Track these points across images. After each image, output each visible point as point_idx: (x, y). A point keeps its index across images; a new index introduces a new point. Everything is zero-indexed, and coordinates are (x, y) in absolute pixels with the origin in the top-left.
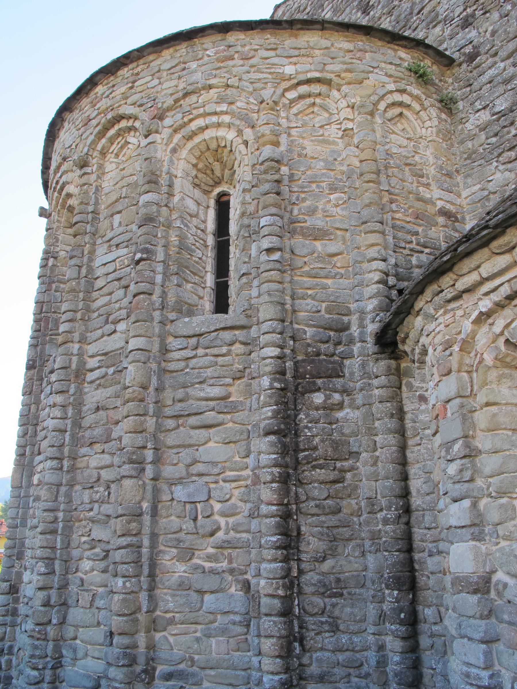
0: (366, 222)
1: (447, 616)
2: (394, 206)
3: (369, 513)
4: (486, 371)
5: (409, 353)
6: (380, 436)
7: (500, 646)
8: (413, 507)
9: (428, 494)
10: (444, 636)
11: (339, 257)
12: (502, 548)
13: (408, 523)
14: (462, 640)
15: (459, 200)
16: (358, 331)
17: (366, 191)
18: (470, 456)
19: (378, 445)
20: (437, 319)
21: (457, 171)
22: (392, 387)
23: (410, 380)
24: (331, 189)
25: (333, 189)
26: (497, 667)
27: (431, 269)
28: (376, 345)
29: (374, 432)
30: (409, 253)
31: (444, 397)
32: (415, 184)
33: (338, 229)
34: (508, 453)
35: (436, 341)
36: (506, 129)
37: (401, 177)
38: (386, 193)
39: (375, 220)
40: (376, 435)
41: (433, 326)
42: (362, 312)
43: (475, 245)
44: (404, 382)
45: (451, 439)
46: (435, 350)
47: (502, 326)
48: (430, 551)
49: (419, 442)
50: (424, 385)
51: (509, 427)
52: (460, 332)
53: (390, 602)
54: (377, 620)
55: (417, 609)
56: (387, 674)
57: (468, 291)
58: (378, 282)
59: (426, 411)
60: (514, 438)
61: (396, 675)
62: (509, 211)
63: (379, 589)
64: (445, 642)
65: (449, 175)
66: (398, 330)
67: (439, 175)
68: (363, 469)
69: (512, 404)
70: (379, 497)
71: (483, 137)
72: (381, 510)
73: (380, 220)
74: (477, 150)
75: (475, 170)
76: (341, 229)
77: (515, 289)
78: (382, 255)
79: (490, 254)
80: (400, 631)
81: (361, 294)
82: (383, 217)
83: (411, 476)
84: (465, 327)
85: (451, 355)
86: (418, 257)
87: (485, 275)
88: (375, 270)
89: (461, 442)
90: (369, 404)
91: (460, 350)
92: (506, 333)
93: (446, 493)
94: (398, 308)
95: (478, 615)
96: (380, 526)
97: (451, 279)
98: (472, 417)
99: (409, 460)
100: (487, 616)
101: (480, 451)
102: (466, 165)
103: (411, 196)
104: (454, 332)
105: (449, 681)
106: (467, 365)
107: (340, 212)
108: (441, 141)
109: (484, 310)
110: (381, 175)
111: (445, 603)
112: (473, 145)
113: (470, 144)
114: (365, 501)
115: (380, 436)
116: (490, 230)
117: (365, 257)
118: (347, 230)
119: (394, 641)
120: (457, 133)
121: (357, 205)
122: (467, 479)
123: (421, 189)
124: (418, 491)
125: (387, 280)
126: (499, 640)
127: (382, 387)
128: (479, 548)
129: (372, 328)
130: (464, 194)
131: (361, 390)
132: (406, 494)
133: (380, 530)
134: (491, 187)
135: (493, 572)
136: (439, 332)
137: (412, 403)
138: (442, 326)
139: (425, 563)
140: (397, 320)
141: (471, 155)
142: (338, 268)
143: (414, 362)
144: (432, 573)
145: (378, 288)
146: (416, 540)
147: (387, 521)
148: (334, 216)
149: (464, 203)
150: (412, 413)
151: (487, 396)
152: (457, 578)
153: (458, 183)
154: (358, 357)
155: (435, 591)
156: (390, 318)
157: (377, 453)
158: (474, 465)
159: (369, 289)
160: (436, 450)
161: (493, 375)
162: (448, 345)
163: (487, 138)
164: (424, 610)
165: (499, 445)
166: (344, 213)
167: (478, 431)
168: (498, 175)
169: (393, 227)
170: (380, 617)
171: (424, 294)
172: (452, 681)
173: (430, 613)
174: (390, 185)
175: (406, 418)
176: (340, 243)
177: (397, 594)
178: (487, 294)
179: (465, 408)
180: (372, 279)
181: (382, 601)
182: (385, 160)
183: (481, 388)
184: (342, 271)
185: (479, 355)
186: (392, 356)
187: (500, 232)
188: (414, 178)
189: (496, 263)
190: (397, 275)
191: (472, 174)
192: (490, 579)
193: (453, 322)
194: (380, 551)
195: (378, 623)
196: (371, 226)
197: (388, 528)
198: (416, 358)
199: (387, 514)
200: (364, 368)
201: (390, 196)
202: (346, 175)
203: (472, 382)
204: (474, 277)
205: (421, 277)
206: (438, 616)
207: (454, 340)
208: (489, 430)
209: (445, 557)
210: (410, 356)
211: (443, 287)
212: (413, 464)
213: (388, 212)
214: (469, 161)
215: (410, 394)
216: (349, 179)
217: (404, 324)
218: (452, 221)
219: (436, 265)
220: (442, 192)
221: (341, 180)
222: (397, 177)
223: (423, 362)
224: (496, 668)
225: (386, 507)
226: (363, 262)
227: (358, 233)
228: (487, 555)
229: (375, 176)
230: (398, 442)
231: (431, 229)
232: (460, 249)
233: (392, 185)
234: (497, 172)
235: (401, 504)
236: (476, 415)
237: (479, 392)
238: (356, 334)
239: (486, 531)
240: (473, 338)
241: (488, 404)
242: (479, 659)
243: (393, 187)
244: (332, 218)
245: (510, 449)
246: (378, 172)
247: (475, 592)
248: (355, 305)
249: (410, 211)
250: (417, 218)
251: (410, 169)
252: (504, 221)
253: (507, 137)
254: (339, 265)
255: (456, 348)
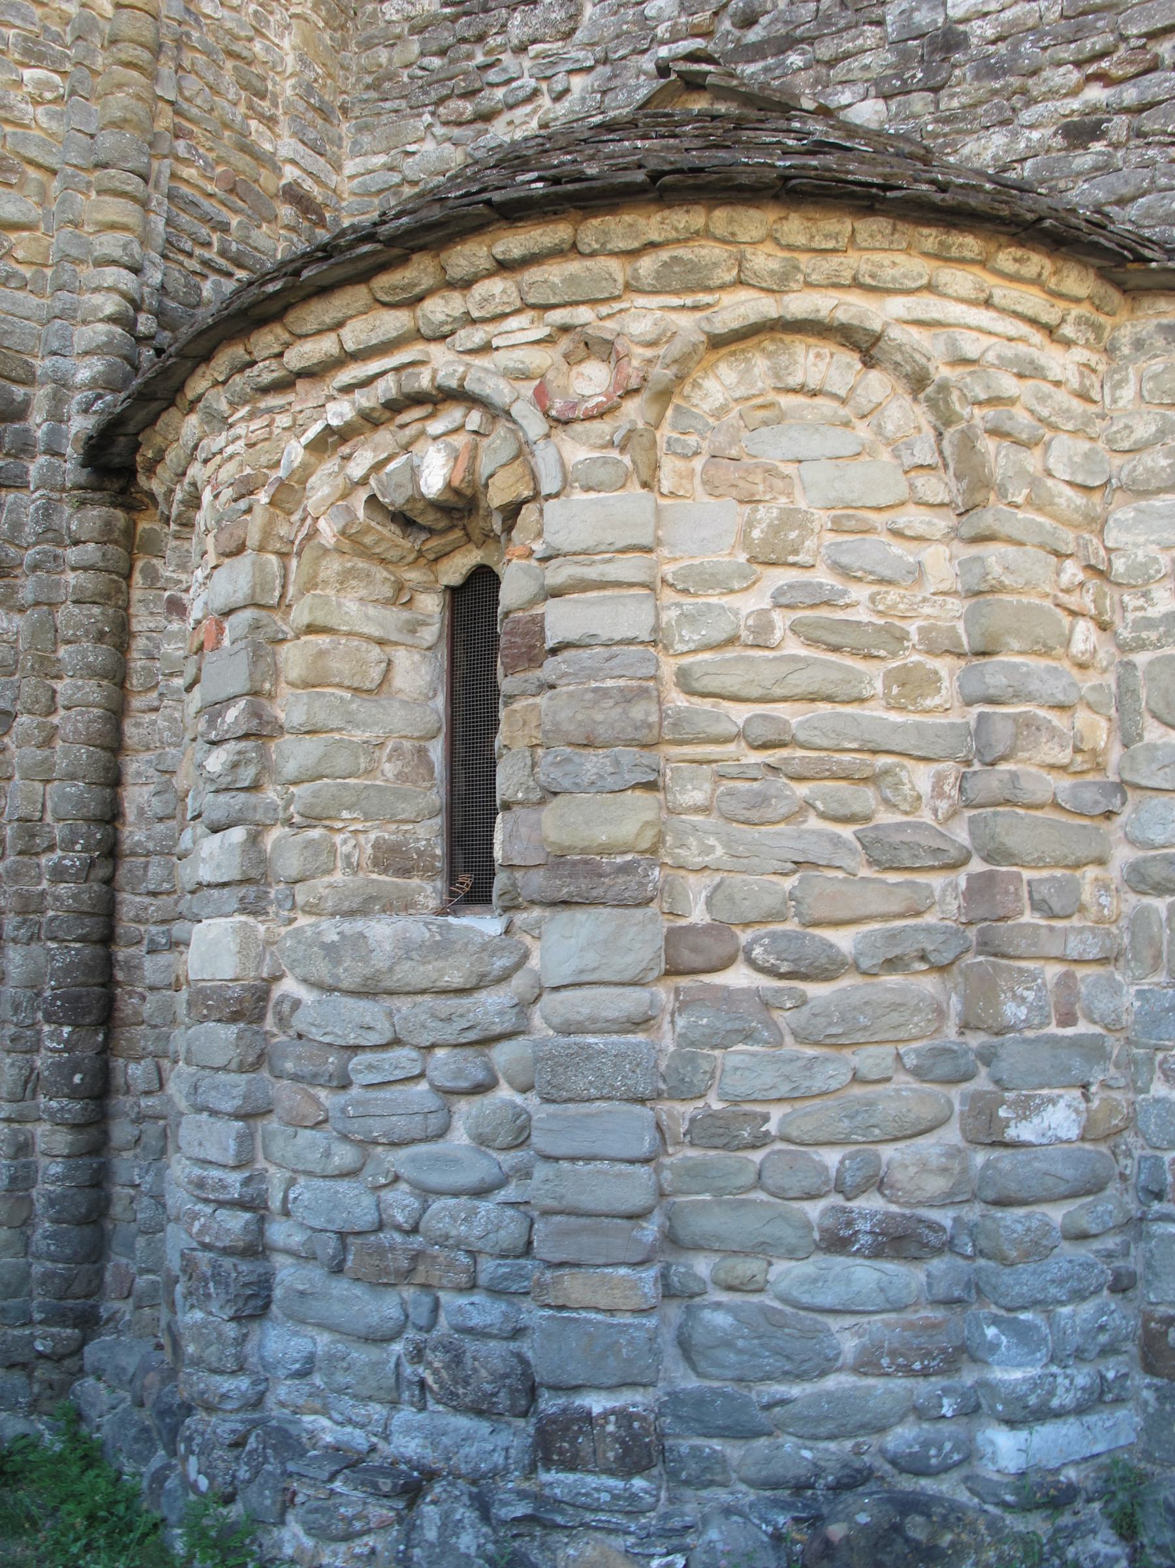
0: (105, 166)
1: (172, 1075)
2: (181, 146)
3: (20, 853)
4: (318, 558)
5: (160, 499)
6: (67, 680)
7: (273, 1124)
8: (126, 846)
9: (161, 819)
10: (165, 1118)
11: (25, 234)
12: (301, 930)
13: (109, 881)
14: (198, 1117)
15: (334, 177)
16: (45, 427)
17: (120, 86)
18: (258, 736)
19: (60, 700)
20: (231, 426)
21: (344, 109)
22: (110, 572)
23: (155, 561)
24: (26, 52)
25: (34, 54)
26: (261, 1164)
27: (235, 306)
28: (83, 466)
29: (54, 671)
30: (198, 268)
31: (220, 603)
32: (242, 109)
33: (31, 162)
34: (337, 736)
35: (224, 474)
36: (467, 46)
37: (211, 79)
38: (168, 109)
39: (129, 165)
40: (59, 677)
41: (221, 440)
42: (62, 384)
43: (340, 273)
44: (139, 565)
45: (222, 696)
46: (216, 497)
47: (368, 466)
48: (152, 941)
49: (156, 704)
50: (183, 577)
51: (347, 683)
52: (277, 464)
53: (52, 1050)
54: (19, 1090)
55: (112, 1065)
56: (32, 1203)
57: (311, 374)
58: (112, 319)
59: (180, 636)
60: (354, 706)
61: (52, 1202)
62: (424, 213)
63: (28, 1021)
64: (165, 1130)
65: (323, 111)
66: (140, 438)
67: (301, 106)
68: (17, 752)
69: (361, 635)
70: (49, 818)
71: (416, 48)
72: (51, 848)
73: (143, 171)
74: (396, 75)
75: (384, 119)
76: (39, 166)
77: (406, 390)
78: (132, 256)
79: (370, 301)
80: (69, 1111)
81: (67, 339)
82: (150, 164)
83: (128, 778)
84: (289, 453)
85: (249, 510)
86: (217, 284)
87: (350, 346)
88: (109, 289)
89: (242, 703)
90: (50, 604)
91: (271, 503)
92: (372, 482)
93: (199, 816)
94: (146, 384)
95: (233, 1066)
96: (45, 885)
97: (277, 339)
98: (274, 654)
99: (129, 742)
100: (252, 1065)
101: (281, 727)
102: (366, 101)
103: (227, 133)
104: (263, 460)
105: (164, 1206)
106: (281, 538)
107: (43, 121)
108: (321, 24)
109: (335, 422)
110: (163, 59)
111: (171, 1048)
112: (390, 60)
113: (383, 55)
114: (15, 824)
115: (67, 680)
116: (379, 246)
117: (90, 252)
118: (54, 172)
119: (54, 1132)
120: (362, 19)
121: (90, 114)
122: (246, 784)
123: (254, 124)
124: (141, 812)
125: (136, 320)
126: (270, 1111)
127: (85, 569)
128: (253, 929)
129: (80, 425)
130: (350, 167)
131: (35, 567)
132: (111, 816)
133: (43, 893)
134: (410, 166)
135: (276, 978)
136: (231, 457)
137: (152, 613)
138: (241, 443)
139: (139, 967)
140: (141, 415)
141: (380, 82)
142: (17, 261)
143: (167, 521)
144: (152, 988)
145: (111, 336)
146: (125, 918)
147: (61, 873)
148: (28, 127)
149: (346, 187)
150: (148, 638)
151: (311, 610)
152: (201, 991)
153: (341, 138)
154: (37, 489)
155: (155, 1027)
156: (125, 405)
157: (55, 720)
158: (263, 755)
159: (87, 330)
160: (189, 721)
161: (332, 567)
162: (246, 489)
163: (423, 54)
164: (126, 1066)
165: (321, 717)
166: (54, 126)
167: (283, 685)
168: (429, 146)
169: (171, 196)
170: (26, 1082)
171: (213, 364)
172: (170, 1202)
173: (139, 1072)
174: (180, 90)
175: (134, 647)
176: (31, 201)
177: (70, 1033)
178: (347, 389)
179: (262, 631)
180: (99, 308)
181: (34, 1049)
182: (180, 23)
183: (302, 593)
184: (27, 272)
185: (309, 521)
186: (120, 500)
187: (397, 257)
188: (243, 94)
189: (378, 323)
190: (159, 314)
191: (375, 127)
192: (268, 992)
193: (266, 439)
194: (39, 939)
195: (19, 1097)
196: (116, 177)
197: (63, 888)
198: (174, 511)
199: (64, 858)
200: (47, 516)
201: (177, 120)
202: (73, 29)
203: (285, 577)
204: (326, 346)
205: (210, 321)
206: (155, 1076)
207: (261, 479)
208: (306, 685)
209: (181, 953)
210: (163, 507)
211: (256, 355)
212: (137, 751)
213: (165, 157)
214: (373, 95)
215: (151, 595)
216: (80, 42)
217: (157, 428)
218: (310, 220)
219: (247, 298)
220: (301, 147)
221: (57, 38)
222: (201, 78)
223: (188, 524)
224: (258, 1166)
225: (63, 841)
226: (82, 262)
227: (82, 186)
228: (268, 943)
229: (146, 56)
230: (107, 697)
231: (259, 227)
232: (306, 274)
233: (187, 93)
234: (429, 137)
235: (98, 836)
236: (285, 650)
237: (298, 600)
238: (39, 433)
239: (272, 896)
240: (303, 482)
241: (311, 629)
242: (226, 1149)
243: (187, 99)
244: (20, 130)
245: (342, 729)
246: (157, 50)
247: (234, 1018)
248: (48, 362)
249: (220, 169)
250: (232, 191)
251: (235, 68)
252: (410, 232)
253: (464, 64)
254: (20, 254)
255: (263, 497)
